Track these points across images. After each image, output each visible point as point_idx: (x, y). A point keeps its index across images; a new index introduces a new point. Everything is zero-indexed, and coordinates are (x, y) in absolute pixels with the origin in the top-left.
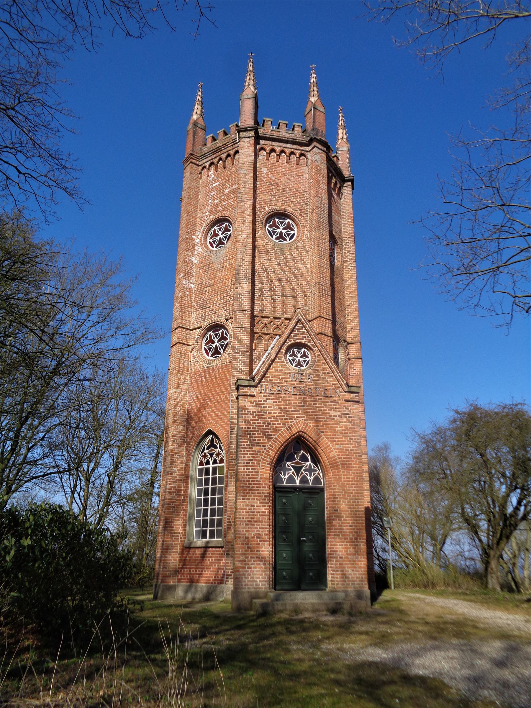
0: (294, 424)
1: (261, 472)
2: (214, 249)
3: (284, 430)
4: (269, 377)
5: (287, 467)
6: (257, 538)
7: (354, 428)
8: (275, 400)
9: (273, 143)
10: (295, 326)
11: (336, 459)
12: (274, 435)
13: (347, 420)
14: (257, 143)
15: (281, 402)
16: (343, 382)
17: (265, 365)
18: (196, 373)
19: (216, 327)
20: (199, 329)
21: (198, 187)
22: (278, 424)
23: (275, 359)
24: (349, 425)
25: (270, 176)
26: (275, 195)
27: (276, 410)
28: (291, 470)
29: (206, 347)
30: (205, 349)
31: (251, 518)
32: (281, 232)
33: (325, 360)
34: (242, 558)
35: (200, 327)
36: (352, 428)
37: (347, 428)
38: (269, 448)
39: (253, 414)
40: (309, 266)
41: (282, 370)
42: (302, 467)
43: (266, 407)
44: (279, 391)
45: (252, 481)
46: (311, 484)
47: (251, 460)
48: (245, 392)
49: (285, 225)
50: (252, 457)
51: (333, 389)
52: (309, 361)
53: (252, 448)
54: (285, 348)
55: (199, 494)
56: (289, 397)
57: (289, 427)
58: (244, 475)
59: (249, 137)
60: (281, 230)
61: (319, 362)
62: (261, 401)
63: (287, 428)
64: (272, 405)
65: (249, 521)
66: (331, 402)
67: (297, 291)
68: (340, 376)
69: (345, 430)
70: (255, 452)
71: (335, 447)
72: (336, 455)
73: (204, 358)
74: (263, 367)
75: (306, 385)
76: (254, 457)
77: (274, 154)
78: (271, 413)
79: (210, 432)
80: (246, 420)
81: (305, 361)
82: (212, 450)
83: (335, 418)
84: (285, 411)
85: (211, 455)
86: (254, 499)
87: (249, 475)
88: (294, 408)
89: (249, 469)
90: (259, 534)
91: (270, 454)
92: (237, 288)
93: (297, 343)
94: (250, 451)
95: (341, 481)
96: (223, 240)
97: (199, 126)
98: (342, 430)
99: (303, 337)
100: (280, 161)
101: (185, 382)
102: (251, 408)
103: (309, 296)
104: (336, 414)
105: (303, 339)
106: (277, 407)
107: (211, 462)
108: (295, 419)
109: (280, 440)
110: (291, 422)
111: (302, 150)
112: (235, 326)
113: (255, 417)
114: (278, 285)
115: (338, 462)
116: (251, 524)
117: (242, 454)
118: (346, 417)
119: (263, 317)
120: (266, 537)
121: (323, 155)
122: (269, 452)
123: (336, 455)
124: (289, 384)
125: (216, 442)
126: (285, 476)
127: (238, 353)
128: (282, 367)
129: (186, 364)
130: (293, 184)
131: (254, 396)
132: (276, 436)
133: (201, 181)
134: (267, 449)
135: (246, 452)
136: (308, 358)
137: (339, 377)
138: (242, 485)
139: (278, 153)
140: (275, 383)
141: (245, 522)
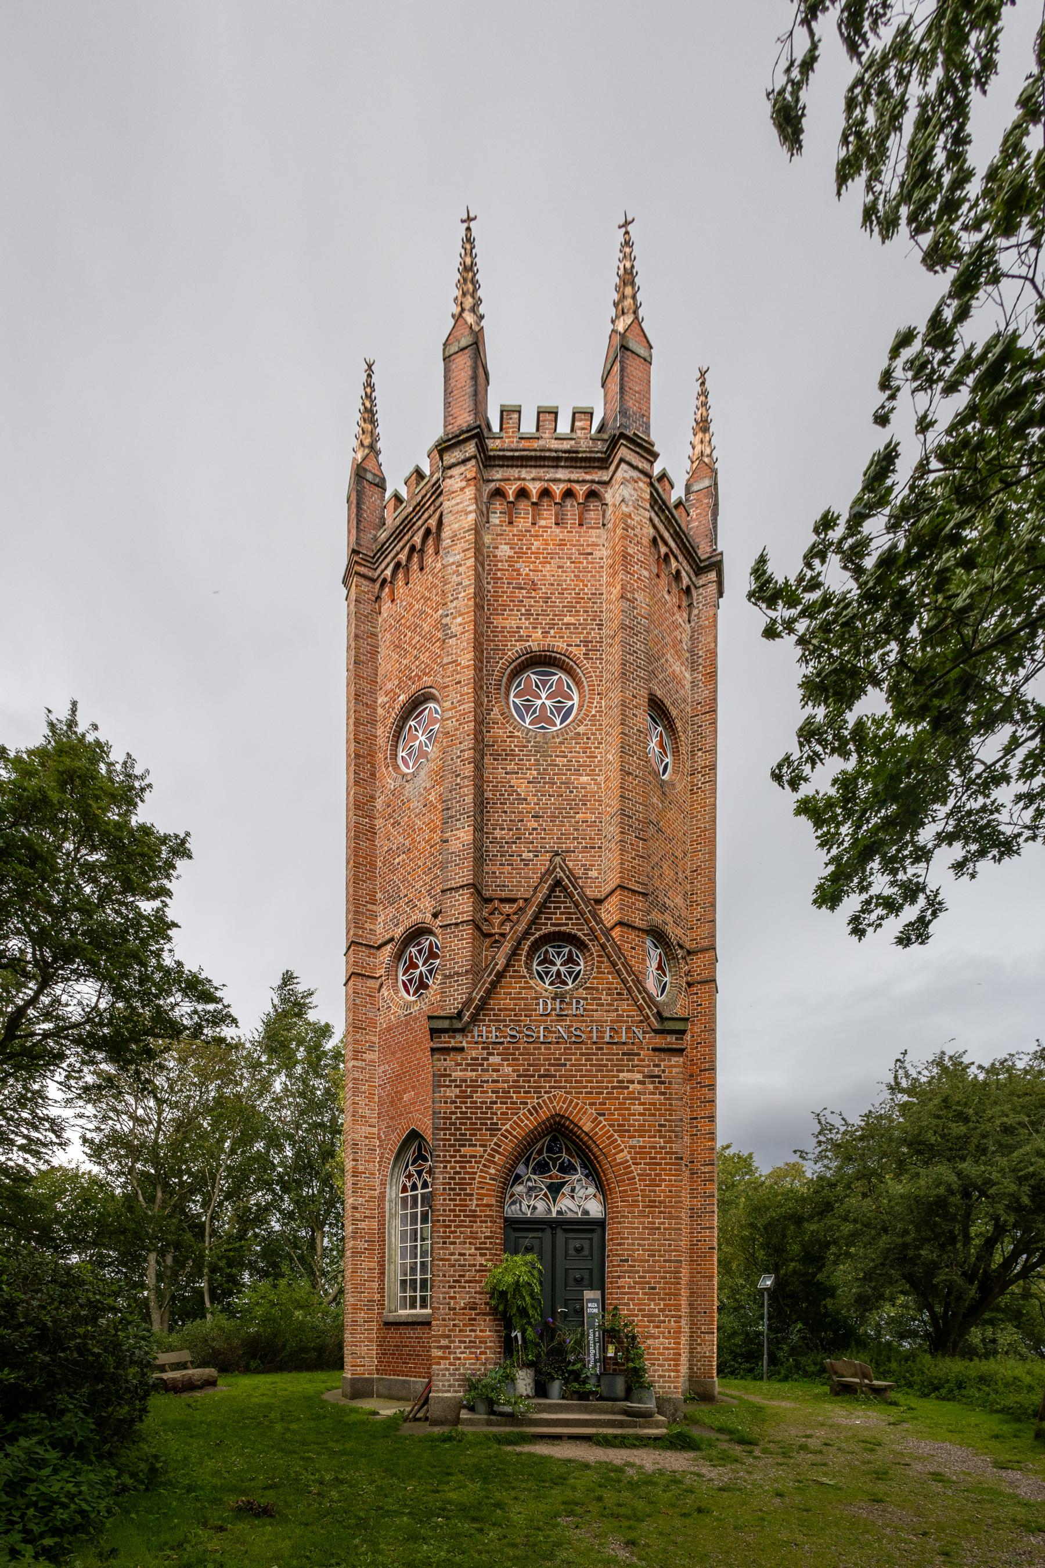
0: (544, 1101)
1: (477, 1194)
3: (524, 1114)
4: (493, 1009)
6: (471, 1309)
7: (670, 1104)
8: (505, 1055)
9: (524, 473)
10: (549, 896)
11: (630, 1166)
12: (503, 1124)
13: (656, 1088)
15: (518, 1059)
17: (484, 984)
18: (389, 1029)
19: (417, 933)
20: (390, 945)
21: (374, 635)
22: (512, 1103)
23: (505, 970)
26: (528, 614)
27: (508, 1076)
29: (404, 978)
30: (404, 982)
31: (460, 1276)
33: (614, 964)
34: (444, 1342)
35: (392, 940)
36: (665, 1104)
37: (654, 1104)
38: (493, 1150)
39: (461, 1086)
40: (601, 779)
41: (520, 993)
44: (513, 1037)
45: (460, 1211)
47: (459, 1173)
48: (445, 1042)
52: (580, 971)
53: (460, 1151)
54: (526, 946)
55: (403, 1240)
56: (535, 1049)
57: (534, 1108)
58: (444, 1200)
59: (464, 462)
61: (599, 973)
62: (477, 1059)
63: (529, 1110)
64: (499, 1065)
65: (454, 1281)
66: (624, 1054)
67: (574, 839)
68: (643, 998)
69: (650, 1109)
70: (466, 1156)
71: (628, 1142)
72: (628, 1158)
73: (402, 998)
74: (480, 990)
75: (571, 1021)
77: (523, 505)
78: (497, 1081)
80: (448, 1097)
83: (631, 1086)
84: (526, 1076)
85: (419, 1173)
86: (465, 1243)
87: (455, 1200)
88: (545, 1070)
89: (454, 1189)
90: (475, 1303)
91: (496, 1160)
92: (447, 841)
93: (554, 933)
94: (455, 1156)
97: (369, 476)
98: (644, 1109)
99: (567, 919)
101: (371, 1049)
102: (457, 1074)
103: (600, 848)
104: (633, 1078)
105: (567, 925)
106: (510, 1069)
108: (545, 1092)
109: (515, 1133)
111: (593, 482)
112: (445, 923)
113: (466, 1092)
114: (534, 829)
116: (460, 1287)
117: (441, 1162)
118: (653, 1082)
119: (502, 900)
122: (494, 1157)
123: (628, 1158)
124: (535, 1021)
125: (426, 1151)
127: (450, 976)
129: (370, 1015)
130: (568, 579)
131: (462, 1049)
132: (508, 1126)
133: (380, 620)
134: (489, 1151)
135: (448, 1158)
136: (579, 965)
137: (641, 1001)
138: (441, 1218)
139: (535, 500)
140: (505, 1021)
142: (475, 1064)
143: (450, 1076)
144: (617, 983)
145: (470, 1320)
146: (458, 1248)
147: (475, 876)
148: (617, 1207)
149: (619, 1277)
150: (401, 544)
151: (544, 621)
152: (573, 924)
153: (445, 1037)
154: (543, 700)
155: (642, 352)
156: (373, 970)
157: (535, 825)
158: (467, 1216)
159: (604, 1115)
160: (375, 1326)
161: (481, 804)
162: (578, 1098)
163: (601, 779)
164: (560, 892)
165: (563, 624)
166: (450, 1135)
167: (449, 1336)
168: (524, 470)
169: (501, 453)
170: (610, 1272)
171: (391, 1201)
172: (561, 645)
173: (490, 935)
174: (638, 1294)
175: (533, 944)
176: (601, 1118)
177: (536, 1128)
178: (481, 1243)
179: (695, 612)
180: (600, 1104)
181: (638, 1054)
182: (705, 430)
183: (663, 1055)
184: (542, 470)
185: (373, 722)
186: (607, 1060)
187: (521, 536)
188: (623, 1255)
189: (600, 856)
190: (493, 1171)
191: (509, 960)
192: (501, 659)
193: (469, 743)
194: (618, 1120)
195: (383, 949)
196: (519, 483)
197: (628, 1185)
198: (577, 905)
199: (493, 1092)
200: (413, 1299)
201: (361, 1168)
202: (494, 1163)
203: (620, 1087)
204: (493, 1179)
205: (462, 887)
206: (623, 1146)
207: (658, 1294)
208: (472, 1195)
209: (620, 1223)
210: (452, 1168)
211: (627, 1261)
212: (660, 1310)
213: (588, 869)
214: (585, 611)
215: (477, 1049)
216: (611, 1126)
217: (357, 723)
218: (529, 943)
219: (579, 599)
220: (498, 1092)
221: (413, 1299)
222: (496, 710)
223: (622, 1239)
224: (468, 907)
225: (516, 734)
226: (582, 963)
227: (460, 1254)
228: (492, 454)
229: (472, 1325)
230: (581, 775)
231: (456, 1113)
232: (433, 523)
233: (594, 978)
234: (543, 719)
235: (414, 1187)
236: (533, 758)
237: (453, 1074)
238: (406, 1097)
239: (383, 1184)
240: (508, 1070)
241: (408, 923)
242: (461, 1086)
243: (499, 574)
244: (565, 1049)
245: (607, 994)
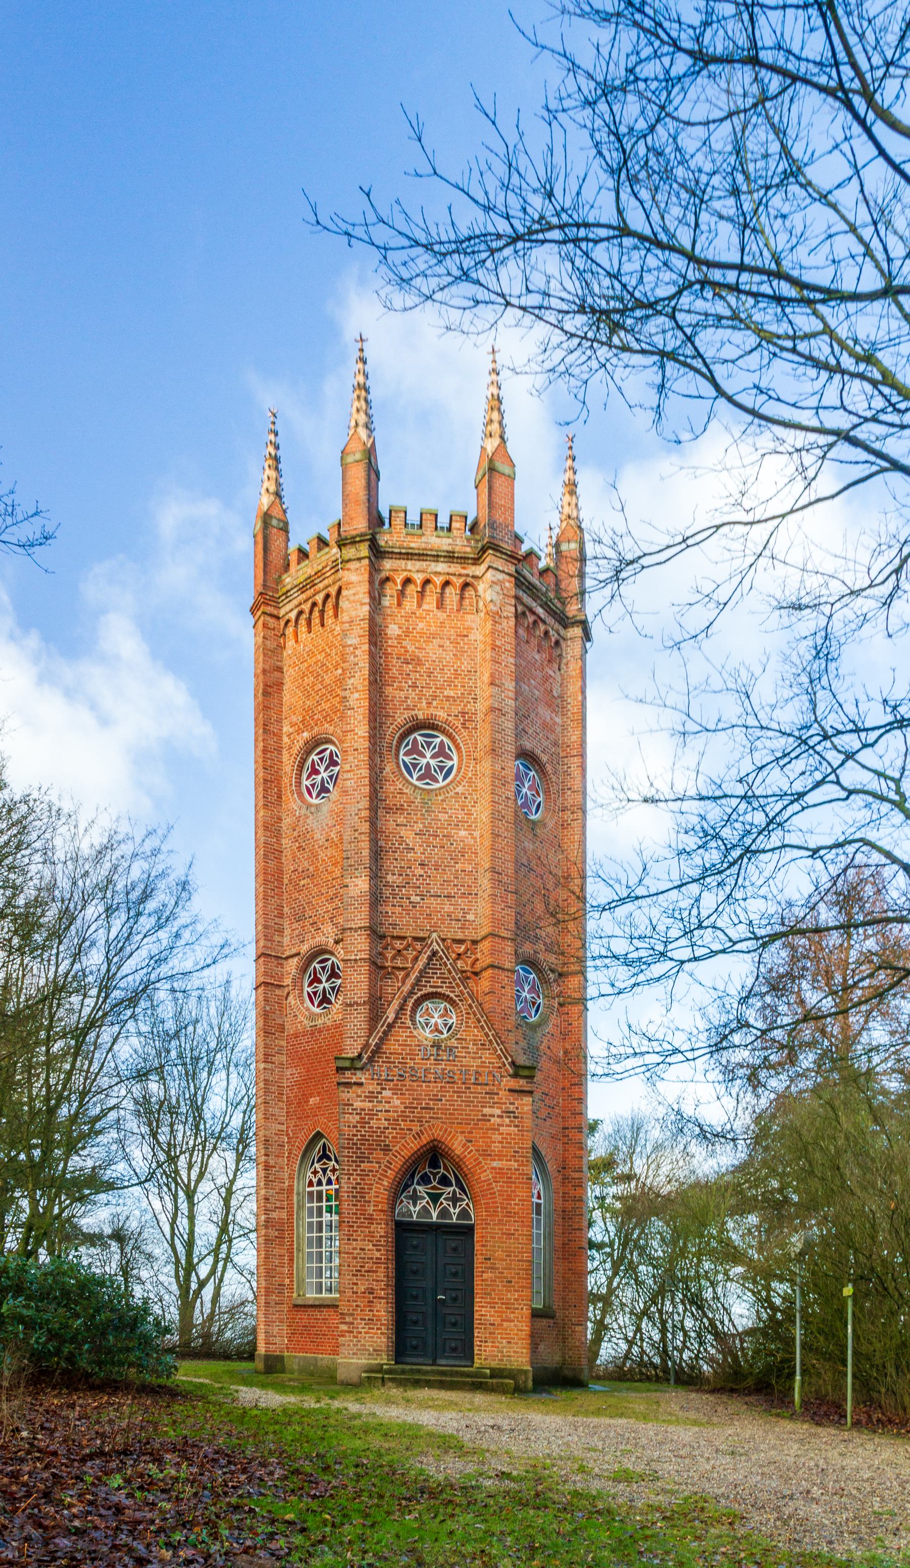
2: (315, 801)
8: (395, 1090)
9: (410, 565)
14: (374, 569)
19: (319, 952)
23: (394, 1022)
25: (404, 643)
26: (414, 686)
28: (424, 1198)
32: (428, 764)
35: (298, 954)
44: (401, 1076)
46: (434, 1219)
51: (490, 1072)
54: (410, 1003)
59: (359, 559)
73: (308, 1009)
82: (325, 1164)
85: (324, 1171)
93: (432, 993)
100: (425, 607)
102: (358, 1104)
111: (467, 575)
126: (415, 1206)
127: (351, 1005)
131: (361, 1084)
142: (371, 1097)
146: (360, 1244)
147: (371, 918)
150: (304, 596)
151: (428, 693)
153: (348, 1074)
154: (428, 759)
156: (281, 978)
157: (422, 872)
160: (285, 1308)
161: (377, 854)
163: (477, 834)
167: (352, 1315)
168: (409, 563)
171: (298, 1194)
172: (442, 714)
173: (383, 968)
175: (416, 1001)
179: (564, 661)
182: (572, 493)
183: (516, 1095)
185: (279, 750)
187: (407, 618)
191: (397, 1014)
193: (365, 803)
195: (290, 960)
196: (405, 574)
198: (450, 972)
201: (272, 1163)
205: (360, 928)
217: (265, 751)
219: (456, 674)
222: (388, 769)
224: (365, 946)
227: (361, 1249)
232: (333, 591)
234: (427, 775)
235: (320, 1183)
238: (312, 1101)
239: (291, 1178)
241: (312, 942)
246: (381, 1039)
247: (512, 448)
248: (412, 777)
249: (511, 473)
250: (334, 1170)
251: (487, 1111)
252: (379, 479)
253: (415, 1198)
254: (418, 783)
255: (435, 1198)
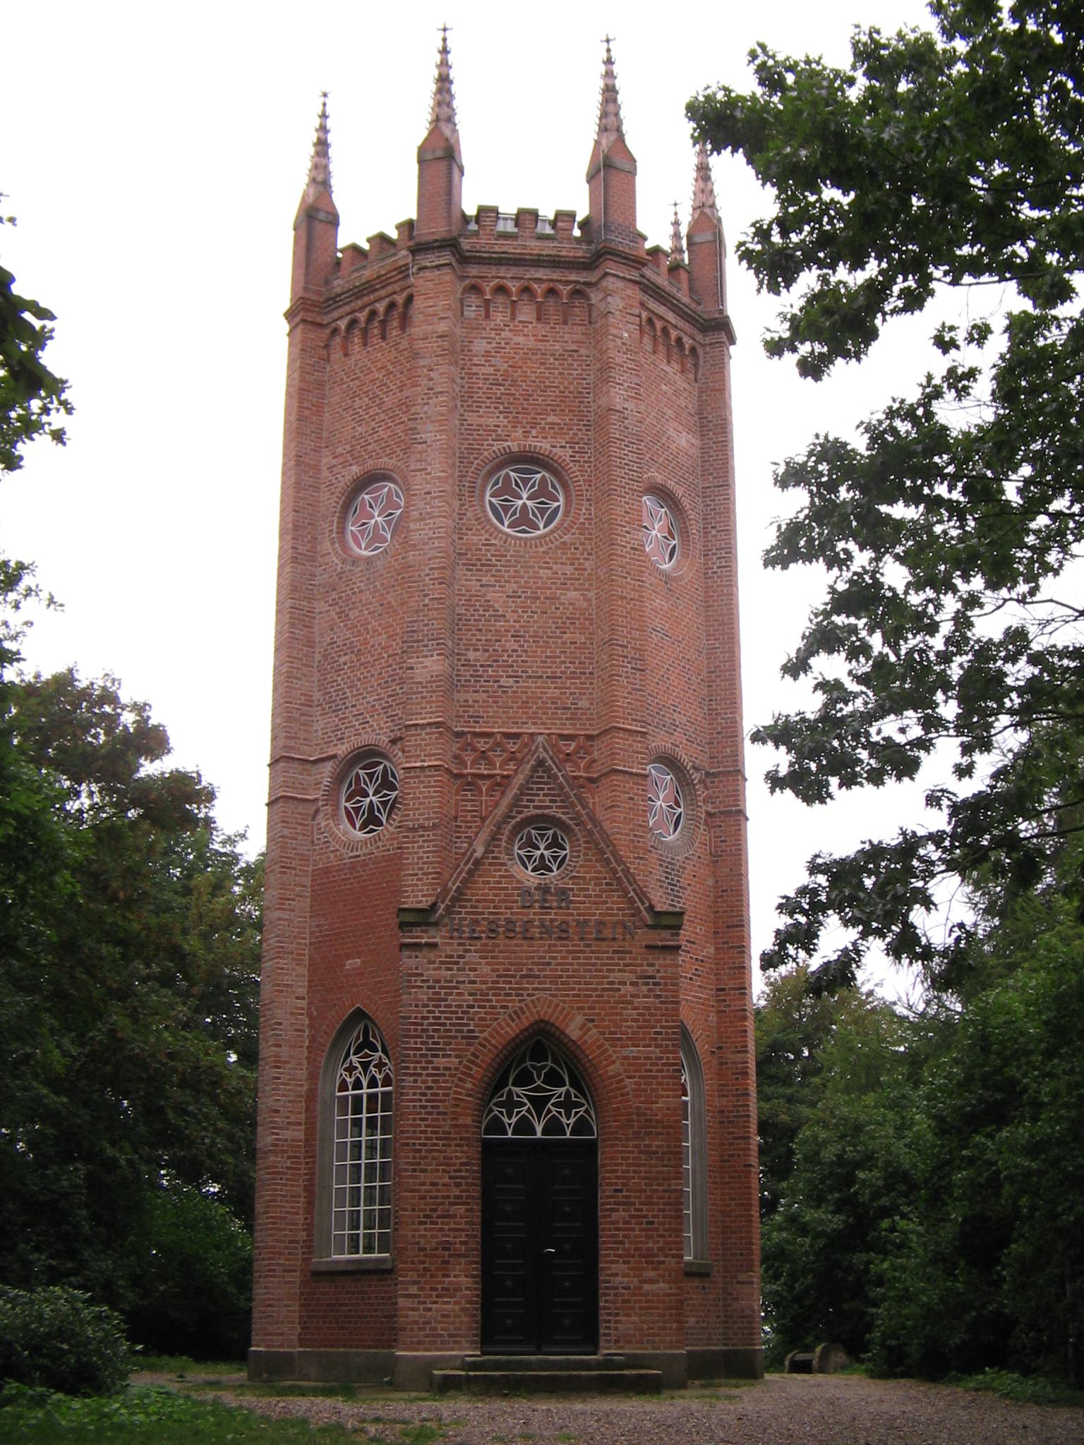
0: (526, 1005)
3: (504, 1020)
5: (516, 1099)
9: (503, 271)
11: (622, 1080)
13: (650, 990)
16: (643, 903)
17: (460, 873)
19: (367, 756)
24: (654, 1003)
27: (487, 975)
31: (432, 1210)
37: (648, 1008)
38: (469, 1061)
40: (591, 594)
42: (549, 1098)
43: (464, 970)
44: (492, 931)
46: (539, 1135)
49: (533, 486)
50: (433, 1081)
57: (515, 1013)
60: (525, 500)
62: (452, 957)
63: (510, 1016)
65: (426, 1216)
76: (437, 1082)
78: (475, 982)
79: (359, 1015)
81: (555, 858)
82: (367, 1056)
84: (506, 976)
92: (412, 668)
93: (537, 816)
94: (426, 1068)
95: (633, 1127)
96: (384, 529)
102: (430, 973)
103: (591, 673)
105: (551, 807)
107: (365, 1084)
110: (521, 1001)
115: (625, 1087)
117: (412, 1075)
120: (463, 1247)
121: (629, 292)
125: (374, 1037)
128: (501, 876)
132: (486, 1034)
137: (632, 894)
138: (411, 1141)
141: (419, 1217)
142: (449, 963)
143: (422, 975)
144: (607, 873)
145: (443, 1262)
148: (609, 1127)
149: (613, 1210)
150: (360, 303)
152: (557, 807)
153: (416, 931)
155: (627, 167)
157: (516, 647)
158: (441, 1139)
159: (593, 1021)
162: (564, 1002)
164: (543, 772)
165: (546, 424)
166: (422, 1043)
169: (478, 254)
170: (603, 1204)
174: (633, 1229)
175: (514, 827)
176: (591, 1025)
177: (517, 1036)
178: (455, 1171)
180: (589, 1008)
181: (630, 952)
184: (522, 269)
186: (597, 958)
188: (616, 1184)
189: (591, 684)
190: (469, 1086)
192: (476, 459)
194: (609, 1027)
197: (621, 1102)
199: (470, 994)
200: (354, 1239)
202: (470, 1076)
203: (611, 989)
204: (469, 1096)
206: (614, 1057)
207: (657, 1230)
208: (445, 1113)
209: (612, 1146)
210: (423, 1082)
211: (621, 1191)
212: (659, 1249)
213: (578, 699)
214: (570, 411)
215: (452, 944)
216: (602, 1033)
217: (298, 486)
218: (509, 827)
220: (476, 994)
221: (354, 1239)
223: (616, 1165)
225: (493, 542)
226: (567, 847)
228: (468, 254)
229: (446, 1269)
230: (568, 589)
231: (428, 1018)
232: (400, 299)
233: (582, 866)
235: (358, 1085)
236: (512, 569)
237: (426, 973)
240: (486, 969)
242: (434, 987)
243: (475, 369)
244: (550, 945)
245: (595, 885)
246: (465, 881)
247: (630, 142)
248: (503, 524)
249: (631, 169)
250: (380, 1066)
251: (614, 976)
252: (462, 174)
253: (511, 1105)
254: (509, 531)
255: (539, 1104)
